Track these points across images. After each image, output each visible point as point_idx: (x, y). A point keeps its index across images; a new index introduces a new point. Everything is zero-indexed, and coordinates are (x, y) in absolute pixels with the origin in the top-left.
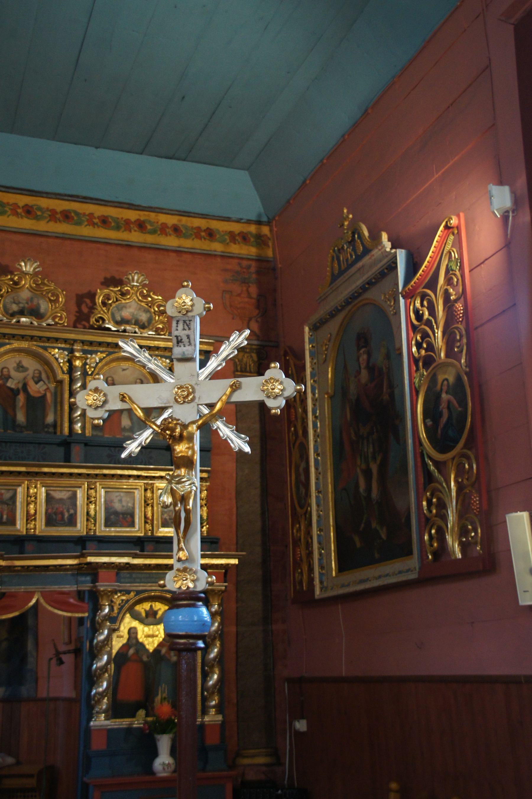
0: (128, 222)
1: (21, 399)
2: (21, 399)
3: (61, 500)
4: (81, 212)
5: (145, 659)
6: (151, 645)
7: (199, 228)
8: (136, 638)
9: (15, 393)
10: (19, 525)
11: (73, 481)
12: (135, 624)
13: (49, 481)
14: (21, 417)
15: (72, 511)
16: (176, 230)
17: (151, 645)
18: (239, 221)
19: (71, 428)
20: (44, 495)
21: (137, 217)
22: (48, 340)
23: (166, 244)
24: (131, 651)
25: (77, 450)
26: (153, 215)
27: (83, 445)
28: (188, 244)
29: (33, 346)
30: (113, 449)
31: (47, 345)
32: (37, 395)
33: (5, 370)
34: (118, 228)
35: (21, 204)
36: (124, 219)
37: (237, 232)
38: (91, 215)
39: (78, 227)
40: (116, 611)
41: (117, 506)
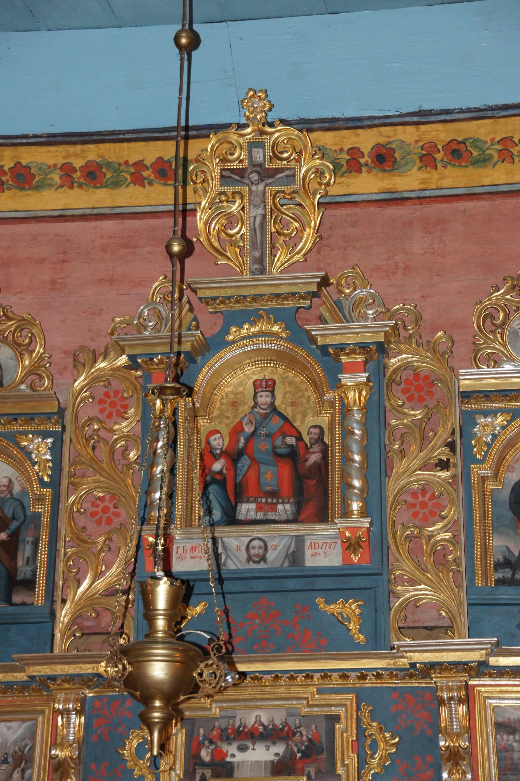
36: (59, 166)
38: (140, 165)
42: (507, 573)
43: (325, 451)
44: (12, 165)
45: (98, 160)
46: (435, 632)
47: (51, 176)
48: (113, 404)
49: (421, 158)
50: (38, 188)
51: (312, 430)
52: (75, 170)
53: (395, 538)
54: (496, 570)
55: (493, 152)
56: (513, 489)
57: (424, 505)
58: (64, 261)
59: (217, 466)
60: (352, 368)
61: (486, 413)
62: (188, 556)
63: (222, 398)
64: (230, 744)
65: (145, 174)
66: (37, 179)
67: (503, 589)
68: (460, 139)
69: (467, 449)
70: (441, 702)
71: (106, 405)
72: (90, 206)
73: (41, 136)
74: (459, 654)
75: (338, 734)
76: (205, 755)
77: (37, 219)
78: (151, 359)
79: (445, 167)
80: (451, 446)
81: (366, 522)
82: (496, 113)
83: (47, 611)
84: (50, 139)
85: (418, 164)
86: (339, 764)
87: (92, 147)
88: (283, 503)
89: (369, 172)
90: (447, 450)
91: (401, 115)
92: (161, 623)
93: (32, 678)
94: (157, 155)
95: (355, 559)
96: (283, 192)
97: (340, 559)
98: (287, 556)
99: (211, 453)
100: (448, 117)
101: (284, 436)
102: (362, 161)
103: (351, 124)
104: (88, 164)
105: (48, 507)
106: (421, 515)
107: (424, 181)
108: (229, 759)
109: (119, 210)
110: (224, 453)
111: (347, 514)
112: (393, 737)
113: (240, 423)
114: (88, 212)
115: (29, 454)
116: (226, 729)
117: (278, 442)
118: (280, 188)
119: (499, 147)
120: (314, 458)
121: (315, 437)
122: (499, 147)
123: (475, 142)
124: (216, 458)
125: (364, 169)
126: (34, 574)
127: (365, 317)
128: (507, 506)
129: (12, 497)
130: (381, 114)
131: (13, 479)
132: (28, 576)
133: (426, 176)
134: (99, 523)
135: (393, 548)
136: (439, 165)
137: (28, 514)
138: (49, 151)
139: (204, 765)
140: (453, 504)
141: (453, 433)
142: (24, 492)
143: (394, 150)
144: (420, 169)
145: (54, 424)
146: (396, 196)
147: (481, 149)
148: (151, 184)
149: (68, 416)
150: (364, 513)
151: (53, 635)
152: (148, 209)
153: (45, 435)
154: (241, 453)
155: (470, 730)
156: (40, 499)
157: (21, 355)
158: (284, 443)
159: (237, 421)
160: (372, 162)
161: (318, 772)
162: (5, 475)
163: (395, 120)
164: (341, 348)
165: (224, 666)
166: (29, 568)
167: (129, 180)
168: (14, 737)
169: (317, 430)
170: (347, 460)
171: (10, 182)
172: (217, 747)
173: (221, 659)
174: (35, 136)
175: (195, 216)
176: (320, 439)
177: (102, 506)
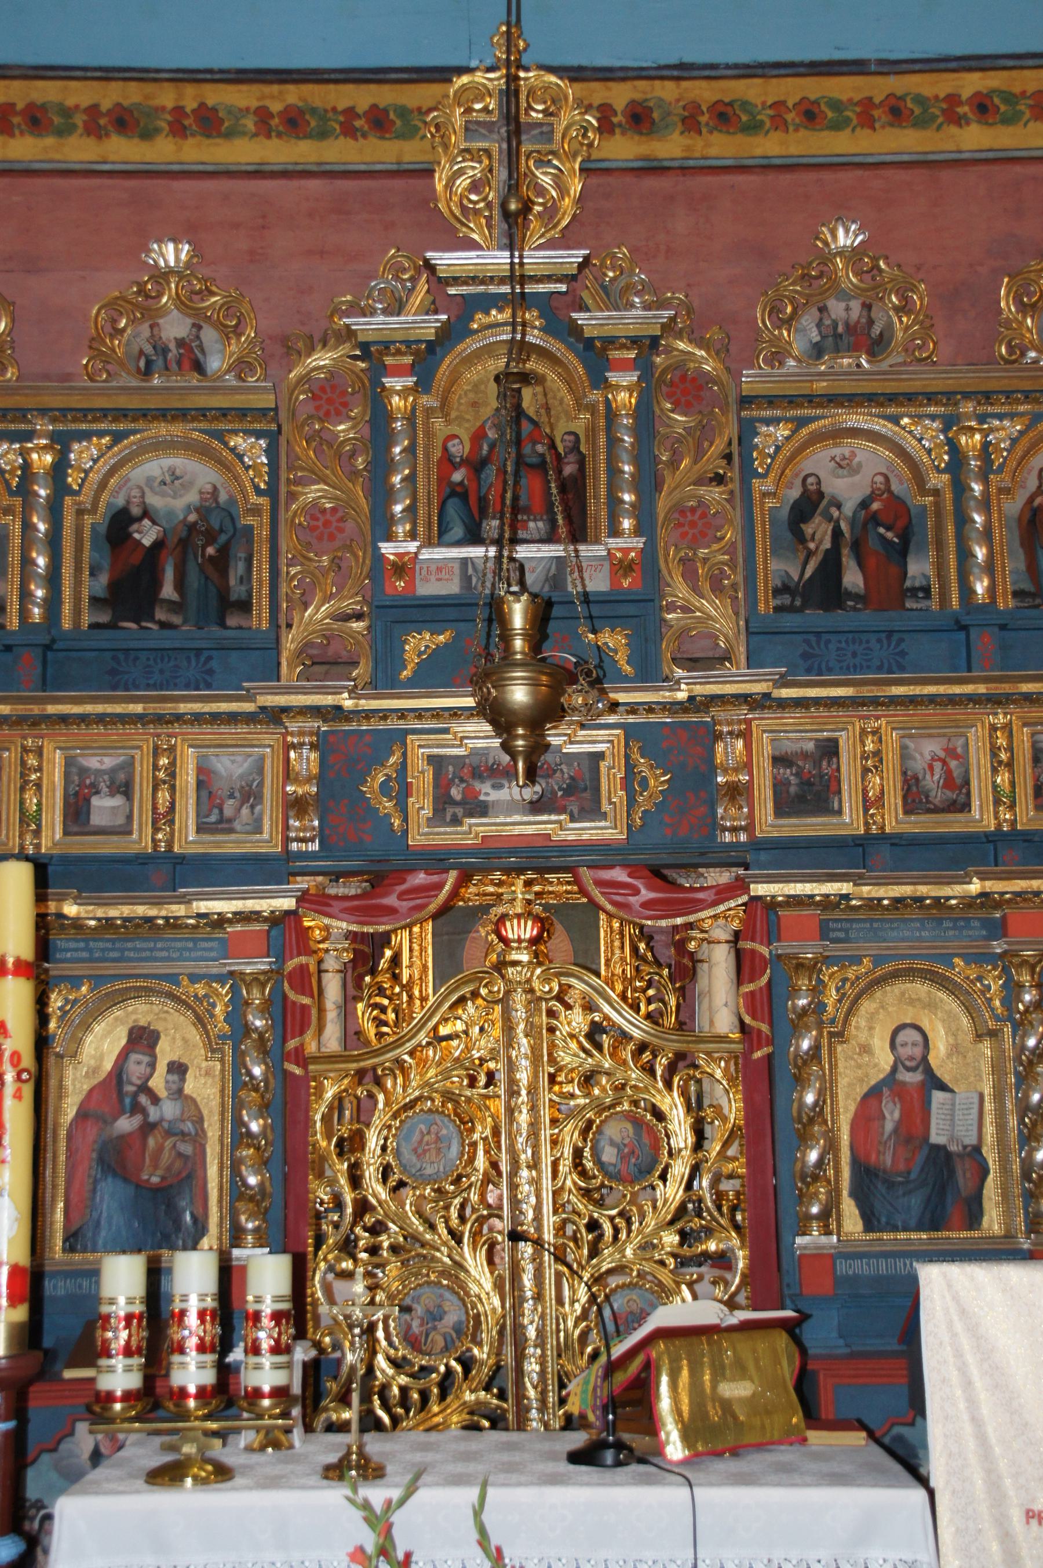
4: (844, 98)
10: (976, 813)
19: (24, 614)
20: (1027, 745)
22: (225, 415)
23: (231, 159)
25: (984, 642)
27: (996, 629)
29: (194, 432)
31: (222, 426)
33: (810, 480)
36: (252, 110)
38: (350, 112)
42: (786, 599)
44: (195, 105)
45: (300, 104)
46: (698, 665)
47: (243, 121)
48: (330, 401)
49: (684, 120)
50: (229, 135)
51: (566, 437)
52: (271, 116)
53: (666, 561)
54: (774, 597)
55: (764, 117)
56: (793, 508)
57: (693, 524)
58: (263, 227)
60: (623, 366)
61: (768, 422)
62: (433, 578)
63: (460, 397)
64: (483, 782)
65: (358, 123)
66: (226, 124)
68: (727, 100)
69: (747, 463)
70: (718, 737)
71: (323, 402)
72: (293, 160)
73: (228, 71)
74: (743, 685)
75: (603, 770)
76: (456, 793)
78: (387, 348)
79: (711, 132)
80: (728, 457)
81: (639, 543)
82: (767, 71)
83: (273, 636)
84: (241, 76)
85: (680, 127)
86: (604, 802)
87: (291, 87)
88: (535, 520)
89: (623, 134)
90: (724, 462)
91: (660, 68)
92: (518, 644)
93: (263, 709)
94: (371, 101)
95: (626, 584)
96: (538, 152)
97: (608, 583)
98: (547, 580)
99: (450, 461)
100: (713, 73)
102: (615, 120)
103: (600, 75)
104: (288, 108)
105: (266, 519)
106: (690, 536)
107: (688, 148)
108: (482, 798)
109: (328, 168)
110: (465, 462)
111: (615, 531)
112: (664, 774)
113: (482, 427)
114: (290, 167)
115: (240, 457)
116: (479, 767)
118: (538, 147)
119: (771, 112)
120: (568, 470)
121: (570, 445)
122: (771, 112)
123: (745, 105)
124: (455, 467)
125: (617, 130)
126: (250, 596)
127: (632, 306)
128: (786, 526)
129: (218, 506)
130: (635, 64)
131: (219, 486)
132: (244, 596)
133: (689, 142)
134: (320, 538)
135: (665, 572)
136: (704, 130)
137: (239, 526)
138: (239, 91)
139: (456, 803)
140: (731, 522)
141: (730, 444)
142: (232, 501)
143: (651, 109)
144: (682, 133)
145: (269, 422)
146: (655, 164)
147: (751, 113)
148: (364, 136)
149: (283, 415)
150: (637, 531)
151: (279, 664)
152: (363, 167)
153: (258, 434)
154: (484, 462)
155: (747, 766)
156: (256, 511)
157: (228, 338)
158: (534, 451)
159: (478, 424)
160: (627, 122)
161: (582, 810)
162: (209, 480)
163: (652, 73)
164: (610, 341)
165: (595, 693)
166: (243, 588)
167: (338, 131)
168: (240, 771)
169: (572, 438)
170: (614, 471)
171: (194, 127)
172: (468, 785)
173: (591, 684)
174: (221, 71)
175: (433, 177)
176: (576, 447)
177: (322, 519)
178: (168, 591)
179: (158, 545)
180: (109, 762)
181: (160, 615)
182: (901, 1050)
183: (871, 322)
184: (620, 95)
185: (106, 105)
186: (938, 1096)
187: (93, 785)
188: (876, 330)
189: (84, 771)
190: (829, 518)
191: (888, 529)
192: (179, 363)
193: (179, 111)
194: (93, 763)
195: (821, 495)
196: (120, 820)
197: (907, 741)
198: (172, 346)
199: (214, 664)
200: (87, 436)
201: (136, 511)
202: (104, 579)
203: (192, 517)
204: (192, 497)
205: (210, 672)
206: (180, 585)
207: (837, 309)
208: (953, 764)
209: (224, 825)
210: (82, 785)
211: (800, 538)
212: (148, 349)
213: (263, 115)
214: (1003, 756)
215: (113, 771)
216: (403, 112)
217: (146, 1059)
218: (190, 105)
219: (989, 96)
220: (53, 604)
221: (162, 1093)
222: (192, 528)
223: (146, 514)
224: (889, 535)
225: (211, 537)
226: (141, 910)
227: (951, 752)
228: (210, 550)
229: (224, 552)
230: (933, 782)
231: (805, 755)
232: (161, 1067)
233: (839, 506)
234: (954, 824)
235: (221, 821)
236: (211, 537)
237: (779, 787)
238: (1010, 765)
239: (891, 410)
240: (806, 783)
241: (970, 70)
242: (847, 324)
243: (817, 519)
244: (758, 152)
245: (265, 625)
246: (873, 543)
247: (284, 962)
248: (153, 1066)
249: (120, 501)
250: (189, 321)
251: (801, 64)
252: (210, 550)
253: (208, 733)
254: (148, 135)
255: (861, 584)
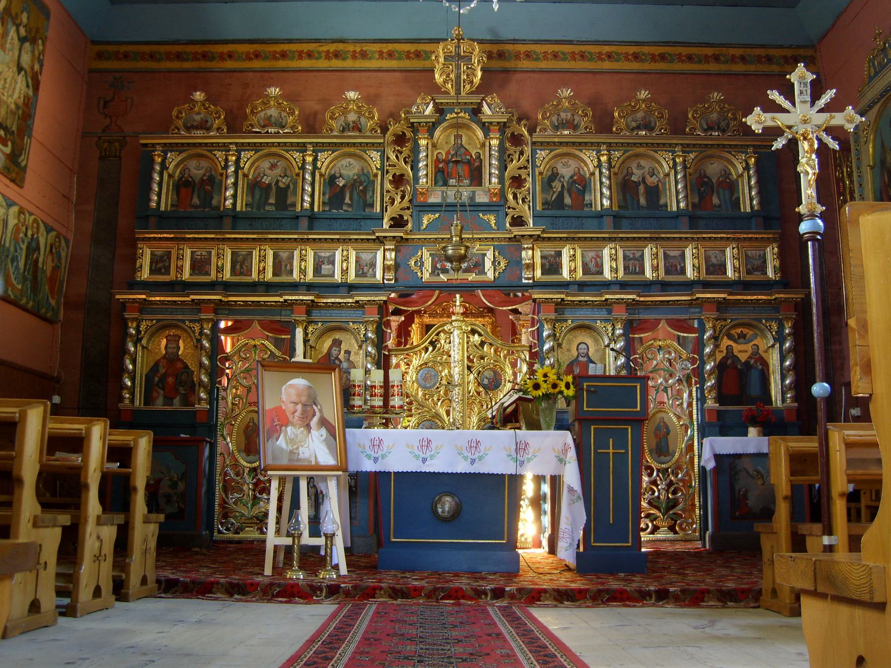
0: (706, 56)
1: (641, 188)
2: (641, 188)
3: (674, 257)
4: (566, 51)
5: (739, 367)
6: (743, 357)
7: (759, 56)
8: (733, 353)
9: (637, 184)
11: (682, 244)
12: (731, 343)
13: (665, 243)
14: (642, 201)
15: (682, 265)
16: (743, 59)
17: (743, 357)
18: (790, 47)
21: (713, 52)
24: (729, 362)
26: (724, 49)
28: (751, 68)
30: (554, 219)
32: (652, 185)
34: (700, 62)
35: (631, 52)
37: (789, 56)
39: (671, 65)
40: (717, 332)
41: (714, 260)
42: (546, 207)
43: (481, 161)
49: (515, 56)
50: (370, 59)
59: (441, 166)
65: (411, 55)
67: (546, 211)
69: (534, 162)
76: (439, 266)
77: (370, 71)
87: (390, 44)
101: (466, 155)
117: (464, 158)
120: (477, 164)
124: (440, 162)
139: (438, 269)
161: (479, 272)
164: (491, 123)
178: (347, 200)
179: (344, 186)
180: (328, 254)
181: (345, 208)
182: (580, 351)
183: (574, 120)
184: (495, 48)
185: (332, 50)
186: (591, 365)
187: (322, 261)
188: (576, 122)
189: (320, 257)
190: (561, 181)
191: (579, 185)
192: (353, 128)
193: (354, 52)
194: (323, 254)
195: (558, 174)
196: (331, 273)
197: (585, 253)
198: (351, 123)
199: (362, 223)
200: (324, 151)
201: (338, 175)
202: (327, 196)
203: (355, 177)
204: (356, 171)
205: (361, 226)
206: (351, 199)
207: (563, 115)
208: (598, 260)
209: (364, 275)
210: (319, 261)
211: (551, 187)
212: (344, 124)
213: (381, 53)
214: (615, 257)
215: (329, 257)
216: (426, 52)
217: (337, 349)
218: (358, 50)
219: (611, 53)
220: (312, 204)
221: (343, 360)
222: (355, 181)
223: (340, 176)
224: (579, 187)
225: (361, 183)
226: (338, 300)
227: (598, 256)
228: (361, 188)
229: (365, 188)
230: (592, 265)
231: (551, 256)
232: (342, 352)
233: (563, 178)
234: (597, 278)
235: (363, 273)
236: (361, 183)
237: (543, 266)
238: (616, 260)
239: (161, 323)
240: (551, 265)
241: (605, 45)
242: (566, 120)
243: (556, 181)
244: (539, 67)
245: (378, 210)
246: (574, 189)
247: (383, 318)
248: (340, 351)
249: (333, 172)
250: (357, 116)
251: (553, 41)
252: (361, 188)
253: (359, 245)
254: (344, 59)
255: (719, 202)
